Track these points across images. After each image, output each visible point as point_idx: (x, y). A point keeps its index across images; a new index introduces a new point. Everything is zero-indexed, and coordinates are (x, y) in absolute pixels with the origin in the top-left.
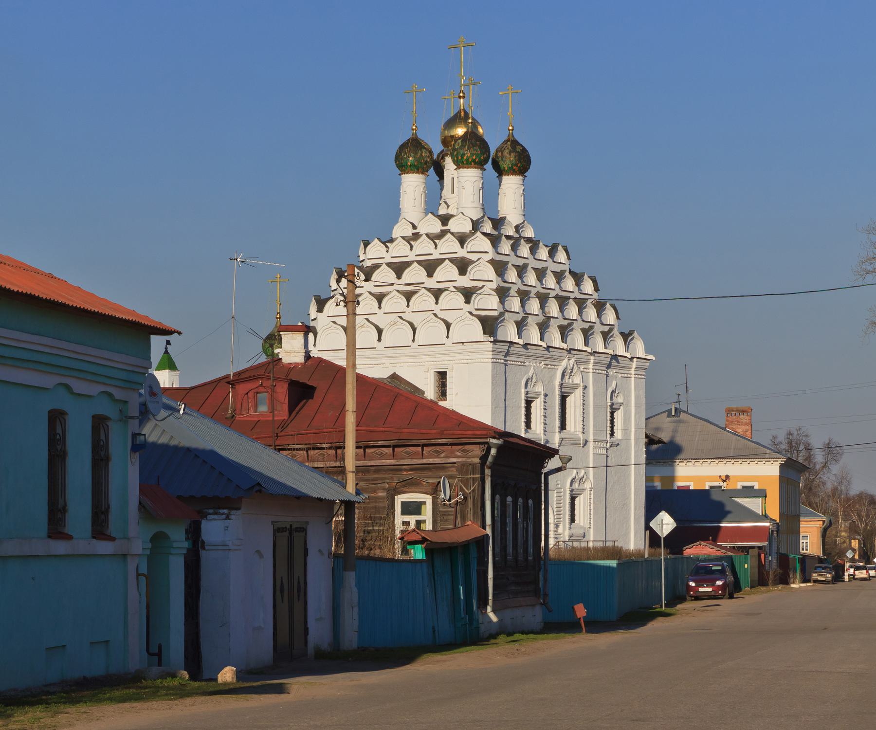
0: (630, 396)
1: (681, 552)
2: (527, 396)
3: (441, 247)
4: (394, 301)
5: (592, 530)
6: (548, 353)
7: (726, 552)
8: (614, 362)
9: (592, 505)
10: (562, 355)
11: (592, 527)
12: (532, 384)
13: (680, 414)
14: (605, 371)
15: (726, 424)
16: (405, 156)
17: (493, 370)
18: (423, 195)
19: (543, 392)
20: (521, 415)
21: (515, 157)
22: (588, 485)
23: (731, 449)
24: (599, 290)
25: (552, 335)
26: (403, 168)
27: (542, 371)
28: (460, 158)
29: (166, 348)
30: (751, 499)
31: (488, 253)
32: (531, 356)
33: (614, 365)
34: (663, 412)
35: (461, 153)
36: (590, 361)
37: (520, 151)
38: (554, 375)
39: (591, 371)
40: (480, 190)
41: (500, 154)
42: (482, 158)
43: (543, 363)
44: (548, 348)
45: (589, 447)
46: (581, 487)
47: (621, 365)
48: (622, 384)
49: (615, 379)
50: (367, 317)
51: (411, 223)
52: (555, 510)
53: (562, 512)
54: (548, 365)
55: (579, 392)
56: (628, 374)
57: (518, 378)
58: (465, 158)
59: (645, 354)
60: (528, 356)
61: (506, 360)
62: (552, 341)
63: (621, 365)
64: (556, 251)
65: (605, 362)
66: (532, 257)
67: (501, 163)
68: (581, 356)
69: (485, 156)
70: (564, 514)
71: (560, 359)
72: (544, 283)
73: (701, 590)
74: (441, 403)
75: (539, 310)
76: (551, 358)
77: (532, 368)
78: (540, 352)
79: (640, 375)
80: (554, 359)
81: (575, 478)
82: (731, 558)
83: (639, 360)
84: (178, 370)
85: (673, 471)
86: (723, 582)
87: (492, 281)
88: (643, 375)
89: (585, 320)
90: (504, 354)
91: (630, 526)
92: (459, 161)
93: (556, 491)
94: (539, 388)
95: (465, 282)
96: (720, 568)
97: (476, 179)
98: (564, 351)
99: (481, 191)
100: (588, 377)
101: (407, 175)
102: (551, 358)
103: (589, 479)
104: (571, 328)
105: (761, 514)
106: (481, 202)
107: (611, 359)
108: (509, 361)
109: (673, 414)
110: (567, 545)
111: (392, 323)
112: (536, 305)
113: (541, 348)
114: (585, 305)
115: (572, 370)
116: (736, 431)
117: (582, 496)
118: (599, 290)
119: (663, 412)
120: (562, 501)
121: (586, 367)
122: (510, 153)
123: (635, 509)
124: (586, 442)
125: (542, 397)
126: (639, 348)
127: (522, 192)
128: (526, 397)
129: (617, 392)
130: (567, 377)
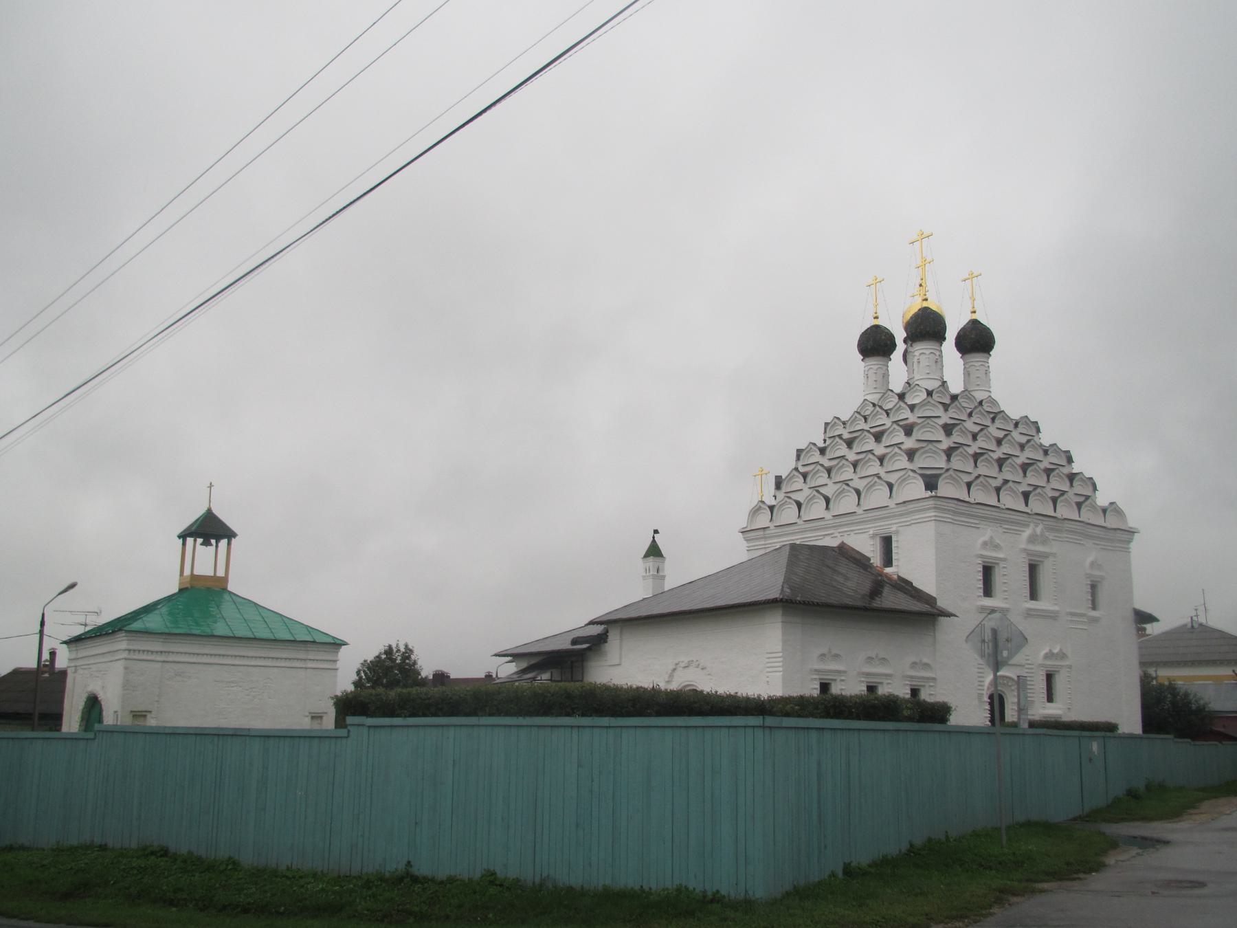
29: (654, 537)
74: (888, 570)
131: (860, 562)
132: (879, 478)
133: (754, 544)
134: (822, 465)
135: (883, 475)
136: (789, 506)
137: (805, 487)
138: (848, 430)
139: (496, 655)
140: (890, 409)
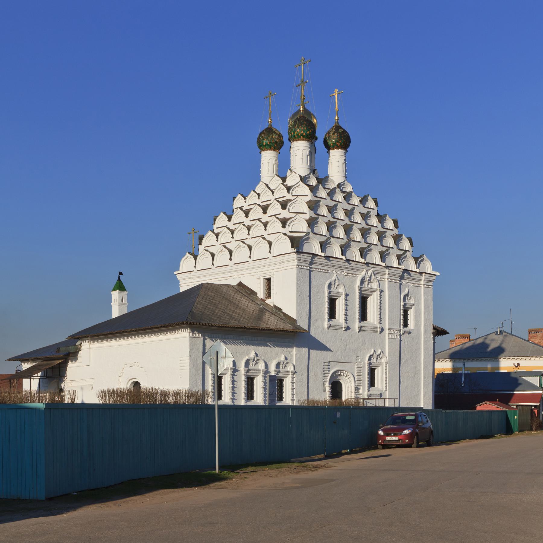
0: (420, 299)
1: (475, 408)
2: (330, 294)
3: (276, 194)
4: (242, 232)
5: (387, 392)
6: (349, 265)
7: (502, 408)
8: (406, 275)
9: (387, 374)
10: (361, 267)
11: (387, 389)
12: (335, 287)
13: (503, 333)
14: (398, 280)
15: (529, 338)
16: (262, 139)
17: (298, 273)
18: (275, 166)
19: (344, 292)
20: (325, 308)
21: (338, 136)
22: (384, 360)
23: (529, 351)
24: (398, 227)
25: (353, 253)
26: (262, 147)
27: (344, 277)
28: (293, 133)
29: (119, 277)
30: (533, 377)
31: (307, 196)
32: (334, 266)
33: (406, 278)
34: (493, 333)
35: (293, 130)
36: (385, 273)
37: (341, 132)
38: (355, 281)
39: (386, 280)
40: (307, 156)
41: (327, 135)
42: (308, 133)
43: (344, 272)
44: (348, 261)
45: (385, 334)
46: (379, 361)
47: (412, 277)
48: (413, 290)
49: (407, 287)
50: (223, 245)
51: (265, 184)
52: (356, 377)
53: (362, 379)
54: (349, 274)
55: (376, 294)
56: (418, 284)
57: (322, 281)
58: (296, 133)
59: (432, 271)
60: (331, 266)
61: (310, 267)
62: (353, 257)
63: (412, 277)
64: (367, 200)
65: (398, 274)
66: (346, 202)
67: (328, 141)
68: (377, 268)
69: (310, 131)
70: (364, 380)
71: (360, 270)
72: (352, 218)
73: (388, 438)
74: (268, 301)
75: (344, 235)
76: (352, 269)
77: (335, 275)
78: (341, 263)
79: (429, 285)
80: (354, 269)
81: (373, 355)
82: (506, 412)
83: (427, 275)
84: (126, 291)
85: (498, 364)
86: (410, 431)
87: (306, 213)
88: (431, 286)
89: (384, 245)
90: (309, 263)
91: (420, 390)
92: (292, 136)
93: (356, 364)
94: (341, 290)
95: (285, 214)
96: (413, 418)
97: (304, 148)
98: (362, 264)
99: (309, 157)
100: (384, 285)
101: (264, 152)
102: (352, 269)
103: (385, 355)
104: (369, 248)
105: (539, 386)
106: (309, 164)
107: (403, 273)
108: (314, 268)
109: (499, 333)
110: (366, 402)
111: (238, 247)
112: (342, 232)
113: (342, 261)
114: (384, 235)
115: (370, 278)
116: (534, 342)
117: (380, 368)
118: (398, 227)
119: (493, 333)
120: (362, 371)
121: (382, 277)
122: (334, 134)
123: (424, 378)
124: (382, 330)
125: (343, 296)
126: (427, 266)
127: (343, 161)
128: (329, 295)
129: (409, 296)
130: (366, 283)
131: (252, 293)
132: (264, 238)
133: (291, 264)
134: (228, 229)
135: (266, 236)
136: (206, 256)
137: (217, 243)
138: (247, 204)
139: (9, 360)
140: (275, 190)
